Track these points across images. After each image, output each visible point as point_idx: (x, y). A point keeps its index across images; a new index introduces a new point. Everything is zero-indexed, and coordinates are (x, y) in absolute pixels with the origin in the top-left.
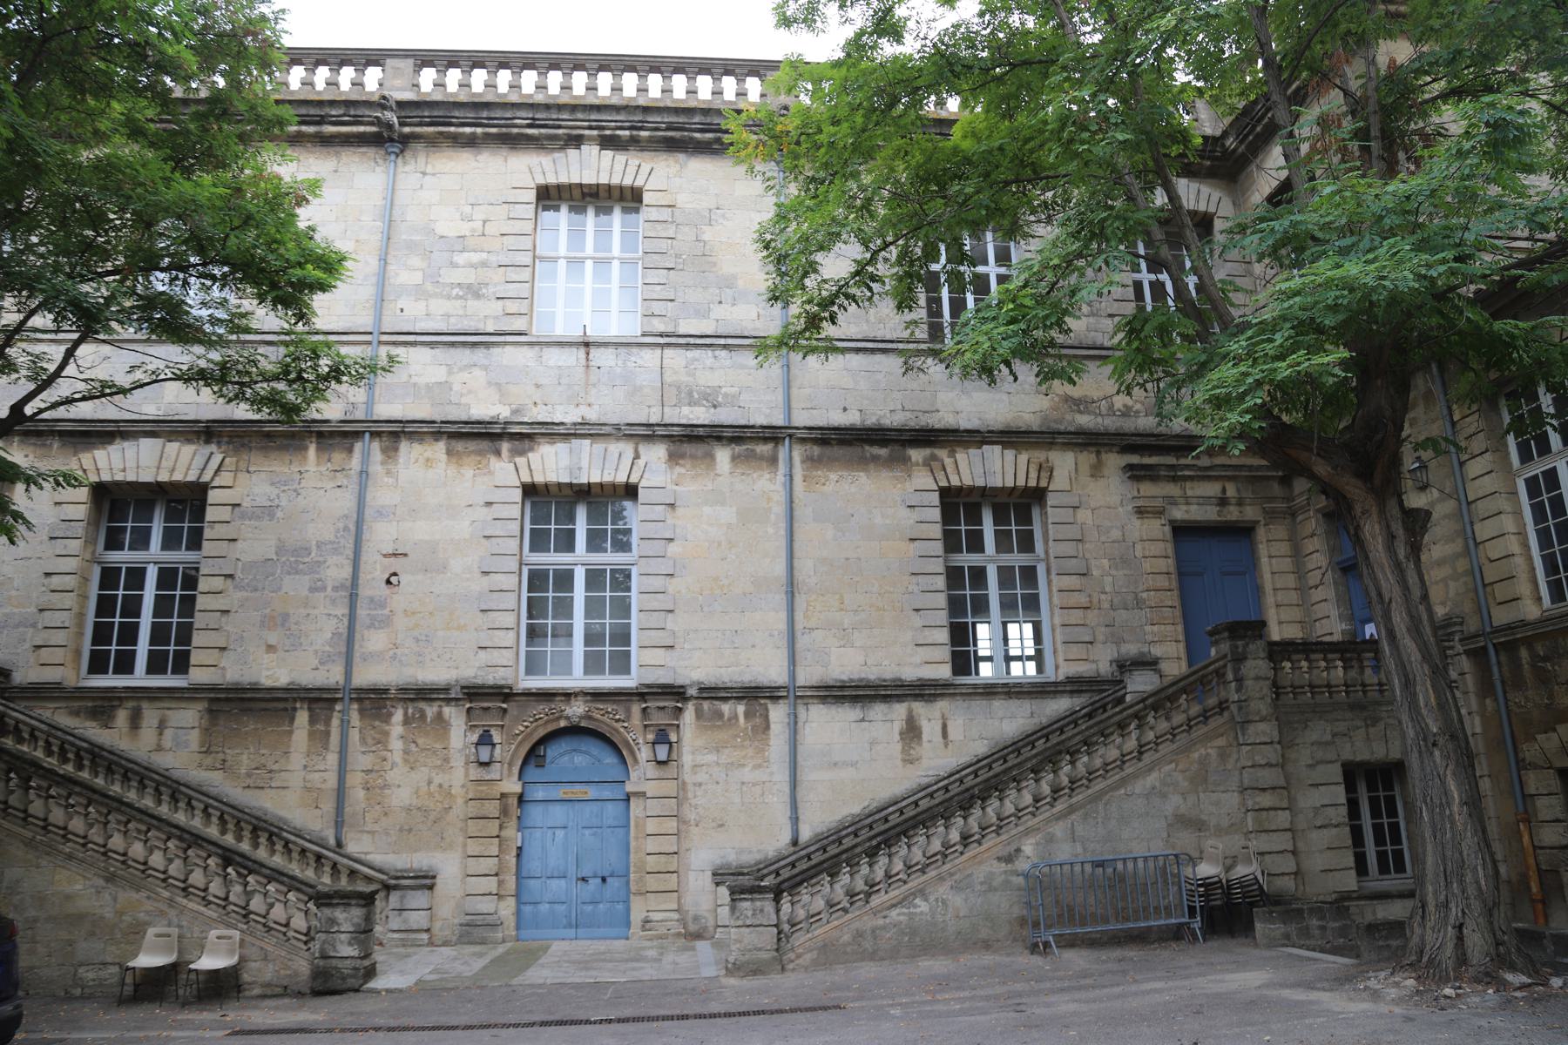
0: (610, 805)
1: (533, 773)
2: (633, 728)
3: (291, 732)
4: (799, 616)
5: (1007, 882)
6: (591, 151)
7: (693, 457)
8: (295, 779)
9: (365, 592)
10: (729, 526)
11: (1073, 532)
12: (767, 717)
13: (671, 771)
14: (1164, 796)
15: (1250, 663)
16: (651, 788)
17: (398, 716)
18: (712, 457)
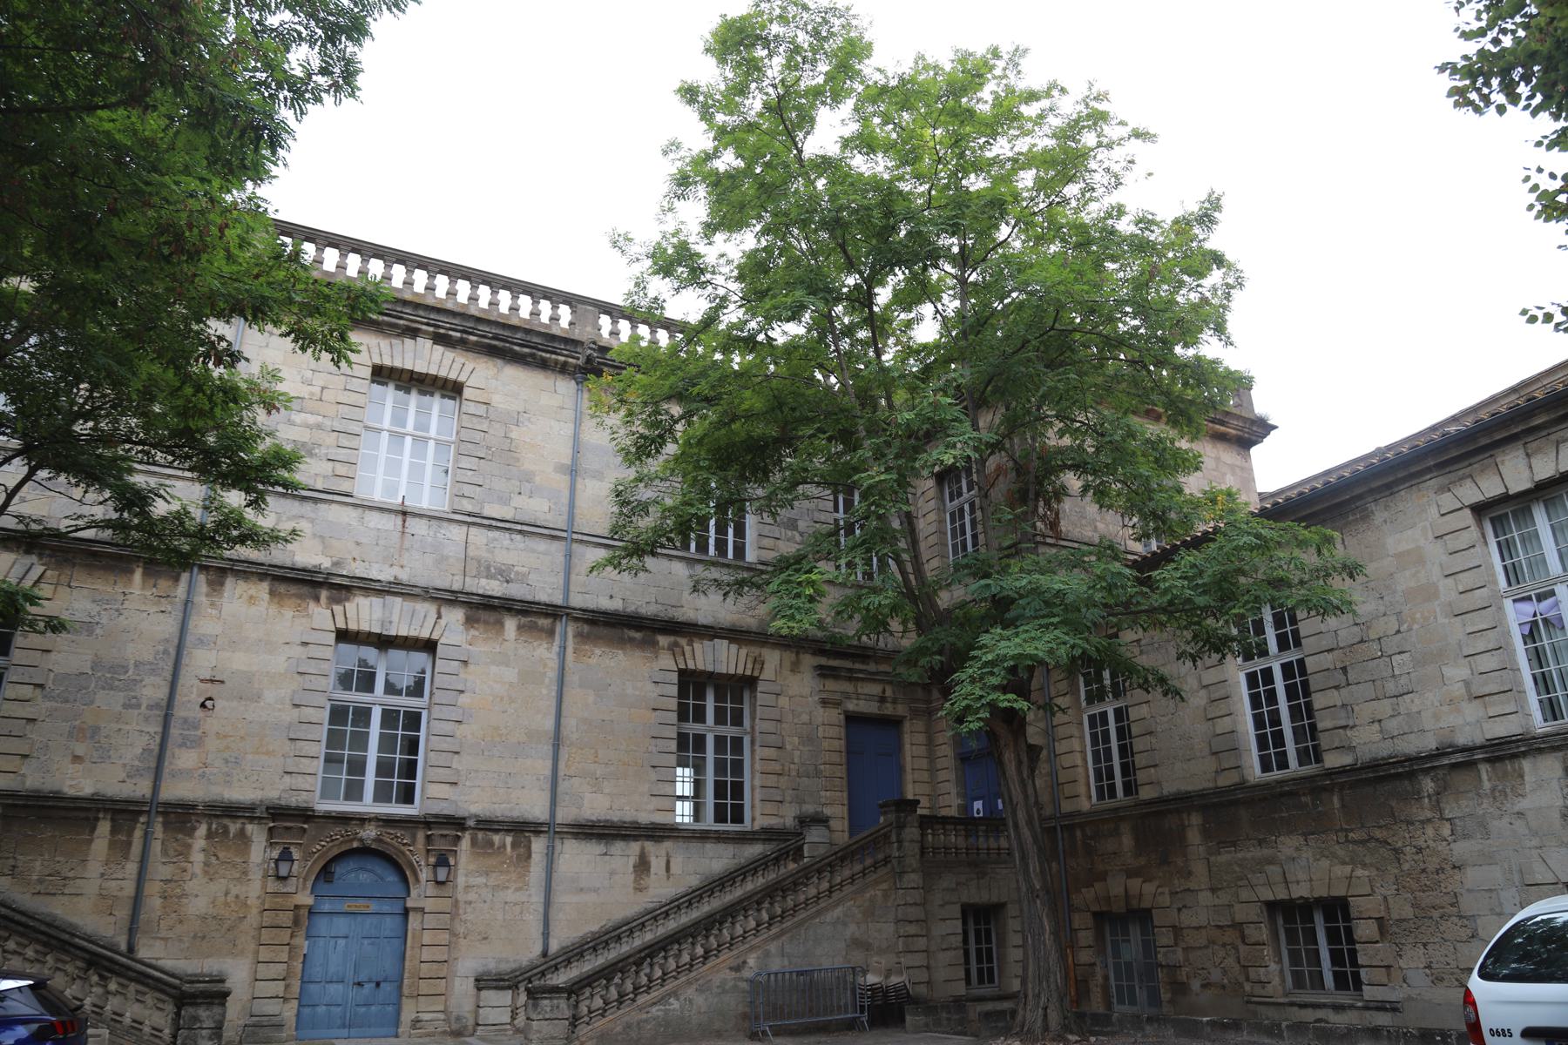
0: (388, 919)
1: (324, 888)
2: (417, 852)
3: (90, 841)
4: (562, 765)
5: (735, 986)
6: (425, 344)
7: (486, 623)
8: (91, 886)
9: (179, 712)
10: (511, 684)
11: (774, 714)
12: (529, 848)
13: (447, 891)
14: (845, 924)
15: (907, 830)
16: (429, 905)
17: (202, 830)
18: (502, 625)
